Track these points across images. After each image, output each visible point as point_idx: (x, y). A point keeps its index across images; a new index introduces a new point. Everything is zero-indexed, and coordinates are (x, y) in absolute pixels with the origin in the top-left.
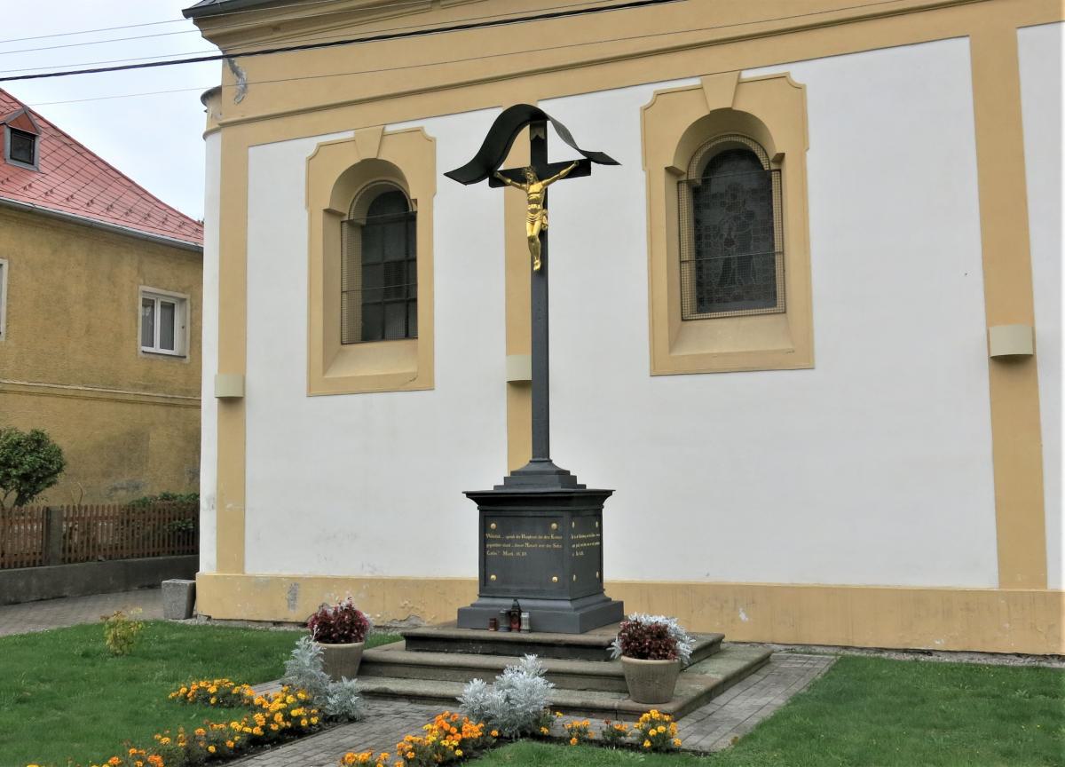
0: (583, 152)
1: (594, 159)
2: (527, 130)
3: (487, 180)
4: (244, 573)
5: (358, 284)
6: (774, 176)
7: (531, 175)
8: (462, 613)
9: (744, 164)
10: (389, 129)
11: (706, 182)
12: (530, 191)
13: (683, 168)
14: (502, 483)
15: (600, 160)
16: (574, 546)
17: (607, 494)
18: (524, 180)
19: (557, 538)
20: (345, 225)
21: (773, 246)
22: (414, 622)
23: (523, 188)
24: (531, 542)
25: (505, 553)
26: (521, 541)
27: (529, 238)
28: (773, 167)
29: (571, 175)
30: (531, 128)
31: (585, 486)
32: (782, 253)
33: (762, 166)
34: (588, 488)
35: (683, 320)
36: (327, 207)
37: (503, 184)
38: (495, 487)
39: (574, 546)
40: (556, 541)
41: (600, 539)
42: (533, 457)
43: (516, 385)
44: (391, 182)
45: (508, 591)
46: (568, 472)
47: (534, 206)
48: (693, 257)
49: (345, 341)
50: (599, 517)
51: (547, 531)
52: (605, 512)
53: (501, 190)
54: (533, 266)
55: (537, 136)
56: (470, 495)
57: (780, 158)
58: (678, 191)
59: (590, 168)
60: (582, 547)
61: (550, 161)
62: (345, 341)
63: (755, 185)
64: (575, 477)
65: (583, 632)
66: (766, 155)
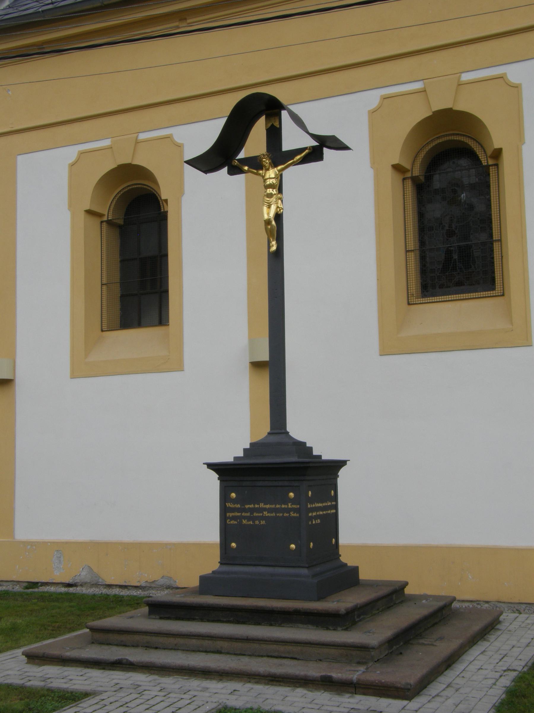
0: (315, 137)
1: (327, 144)
2: (262, 121)
3: (226, 169)
4: (14, 538)
5: (117, 277)
6: (492, 170)
7: (266, 162)
8: (203, 579)
9: (464, 162)
10: (142, 136)
11: (429, 177)
12: (267, 176)
13: (408, 166)
14: (241, 454)
15: (331, 145)
16: (310, 514)
17: (342, 463)
19: (294, 506)
20: (104, 224)
21: (491, 235)
23: (259, 174)
24: (270, 510)
27: (265, 221)
28: (491, 162)
29: (305, 160)
31: (320, 457)
32: (500, 241)
33: (481, 162)
34: (323, 458)
35: (409, 304)
36: (88, 208)
37: (241, 172)
38: (235, 458)
39: (310, 514)
40: (295, 510)
41: (336, 507)
43: (257, 365)
46: (304, 443)
47: (270, 191)
48: (418, 248)
50: (335, 487)
51: (287, 500)
52: (340, 481)
53: (241, 178)
54: (269, 247)
55: (272, 125)
56: (211, 466)
57: (497, 154)
58: (404, 187)
59: (323, 154)
60: (320, 515)
61: (284, 149)
62: (105, 328)
63: (474, 180)
64: (311, 448)
65: (320, 598)
66: (485, 151)
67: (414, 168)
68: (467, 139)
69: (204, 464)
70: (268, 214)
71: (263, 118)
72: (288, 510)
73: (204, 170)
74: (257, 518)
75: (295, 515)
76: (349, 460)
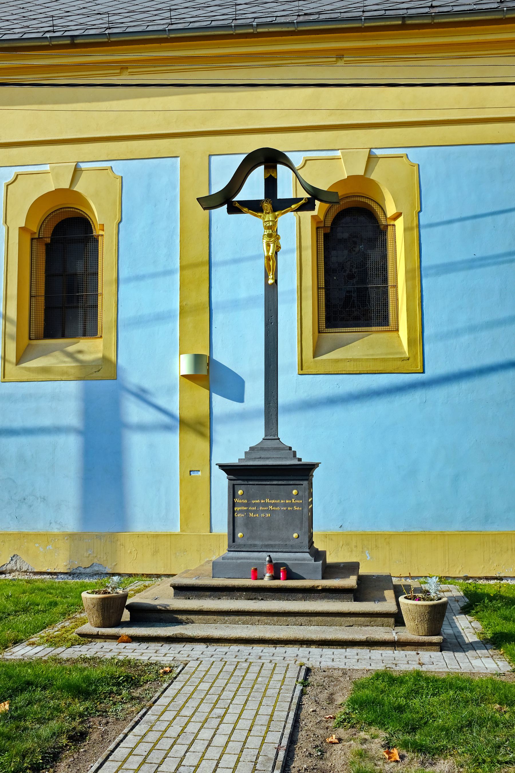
2: (261, 169)
14: (243, 457)
18: (261, 210)
22: (96, 568)
25: (251, 515)
26: (266, 505)
30: (265, 168)
40: (298, 505)
42: (266, 436)
44: (82, 211)
45: (255, 546)
49: (33, 337)
51: (290, 496)
61: (278, 198)
62: (33, 337)
67: (326, 220)
68: (371, 201)
69: (216, 464)
70: (268, 251)
71: (263, 167)
72: (292, 505)
73: (204, 207)
74: (263, 511)
75: (298, 509)
76: (321, 463)
